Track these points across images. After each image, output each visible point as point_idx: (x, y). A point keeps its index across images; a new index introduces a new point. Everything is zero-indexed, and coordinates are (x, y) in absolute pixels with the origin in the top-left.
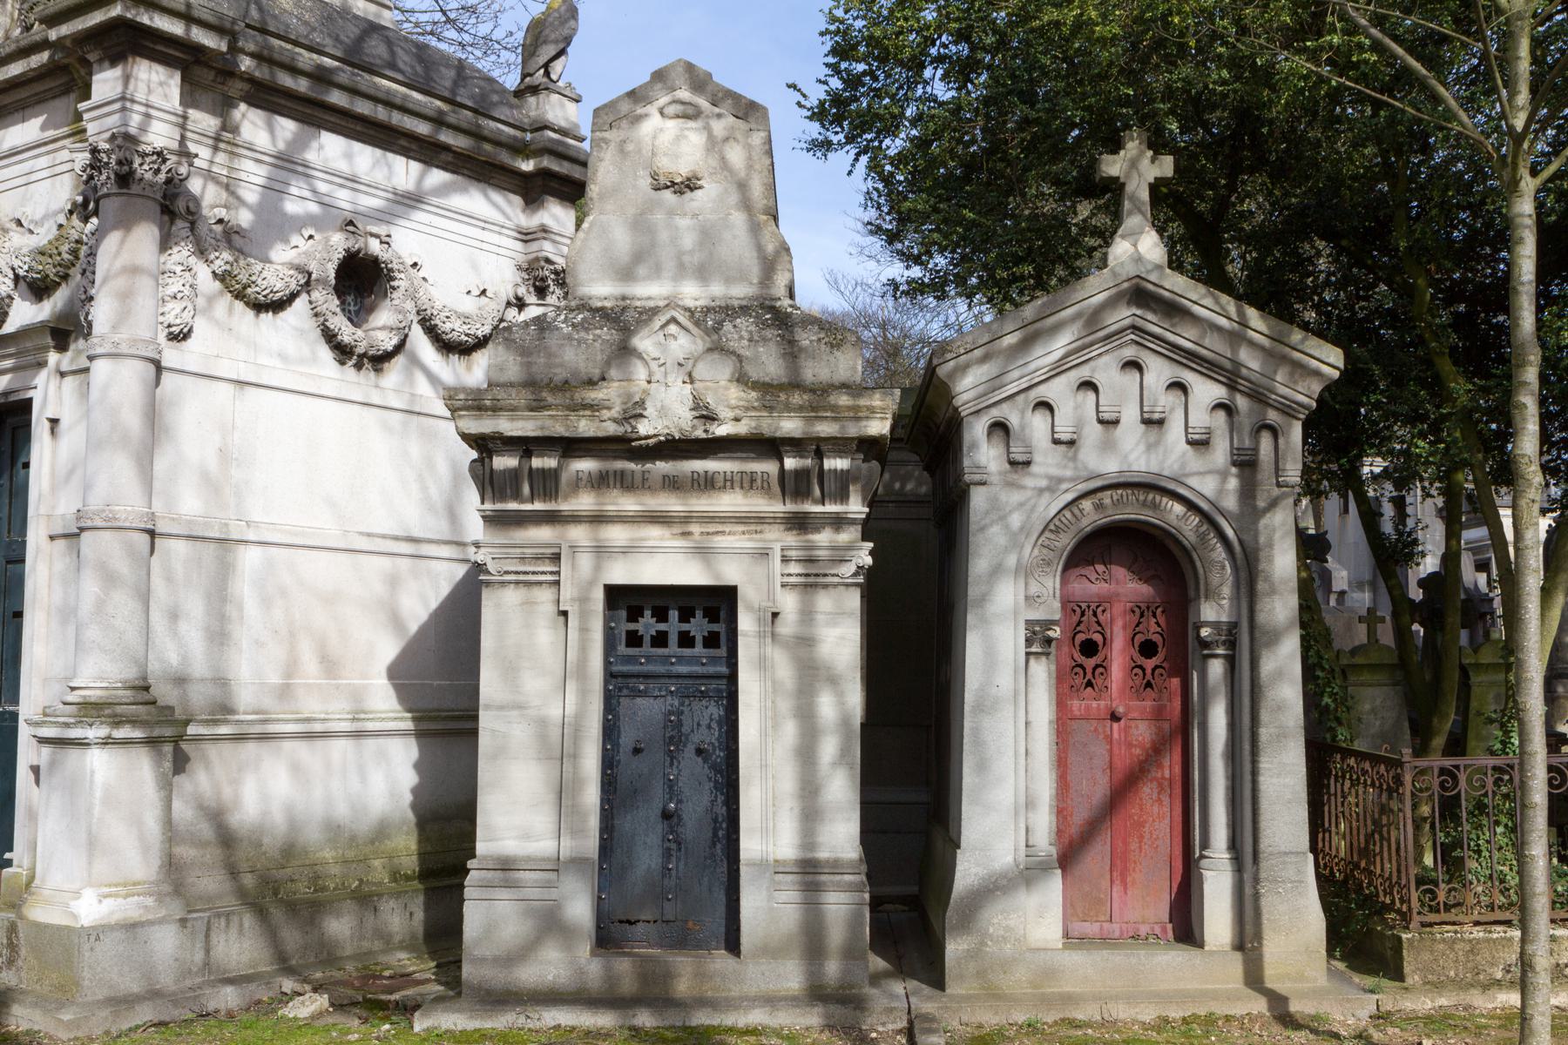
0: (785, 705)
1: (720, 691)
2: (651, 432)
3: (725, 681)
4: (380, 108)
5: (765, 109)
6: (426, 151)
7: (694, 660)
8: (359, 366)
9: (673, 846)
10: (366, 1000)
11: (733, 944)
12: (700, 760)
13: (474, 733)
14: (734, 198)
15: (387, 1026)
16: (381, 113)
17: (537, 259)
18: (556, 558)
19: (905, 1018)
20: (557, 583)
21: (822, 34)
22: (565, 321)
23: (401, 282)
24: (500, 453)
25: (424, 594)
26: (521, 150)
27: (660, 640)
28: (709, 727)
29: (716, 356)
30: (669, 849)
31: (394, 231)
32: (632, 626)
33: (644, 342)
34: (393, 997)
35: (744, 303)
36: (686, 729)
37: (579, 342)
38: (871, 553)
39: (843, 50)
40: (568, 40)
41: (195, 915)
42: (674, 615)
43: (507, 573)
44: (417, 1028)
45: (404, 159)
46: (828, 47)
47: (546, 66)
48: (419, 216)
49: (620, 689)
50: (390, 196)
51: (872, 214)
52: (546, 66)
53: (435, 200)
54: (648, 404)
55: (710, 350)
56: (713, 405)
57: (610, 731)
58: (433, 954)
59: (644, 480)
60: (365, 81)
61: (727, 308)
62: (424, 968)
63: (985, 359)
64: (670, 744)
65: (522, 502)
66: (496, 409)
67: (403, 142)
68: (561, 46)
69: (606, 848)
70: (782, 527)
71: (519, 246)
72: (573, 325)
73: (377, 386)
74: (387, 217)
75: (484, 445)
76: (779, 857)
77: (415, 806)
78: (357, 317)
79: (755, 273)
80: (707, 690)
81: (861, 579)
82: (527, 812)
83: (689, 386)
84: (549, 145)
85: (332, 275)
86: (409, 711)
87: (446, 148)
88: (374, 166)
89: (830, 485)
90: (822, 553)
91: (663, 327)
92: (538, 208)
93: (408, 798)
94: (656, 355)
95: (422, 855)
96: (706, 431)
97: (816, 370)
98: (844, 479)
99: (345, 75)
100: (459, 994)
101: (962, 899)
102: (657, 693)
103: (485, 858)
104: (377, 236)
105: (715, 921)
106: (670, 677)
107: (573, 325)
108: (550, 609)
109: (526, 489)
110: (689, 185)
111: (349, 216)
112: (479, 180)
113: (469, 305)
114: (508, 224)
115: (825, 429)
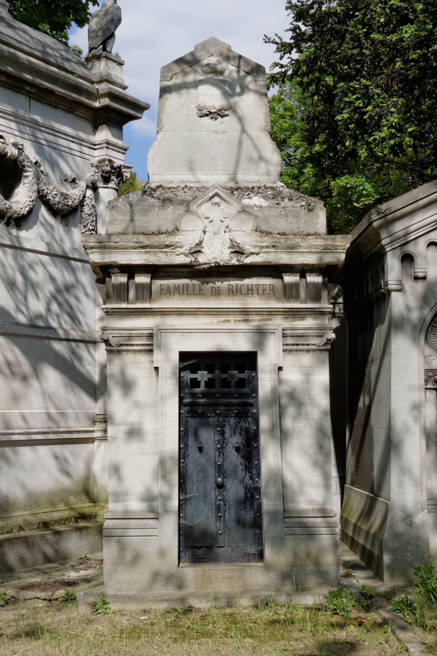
9: (222, 503)
29: (243, 216)
30: (219, 505)
41: (30, 594)
64: (218, 444)
70: (282, 317)
81: (329, 347)
96: (238, 260)
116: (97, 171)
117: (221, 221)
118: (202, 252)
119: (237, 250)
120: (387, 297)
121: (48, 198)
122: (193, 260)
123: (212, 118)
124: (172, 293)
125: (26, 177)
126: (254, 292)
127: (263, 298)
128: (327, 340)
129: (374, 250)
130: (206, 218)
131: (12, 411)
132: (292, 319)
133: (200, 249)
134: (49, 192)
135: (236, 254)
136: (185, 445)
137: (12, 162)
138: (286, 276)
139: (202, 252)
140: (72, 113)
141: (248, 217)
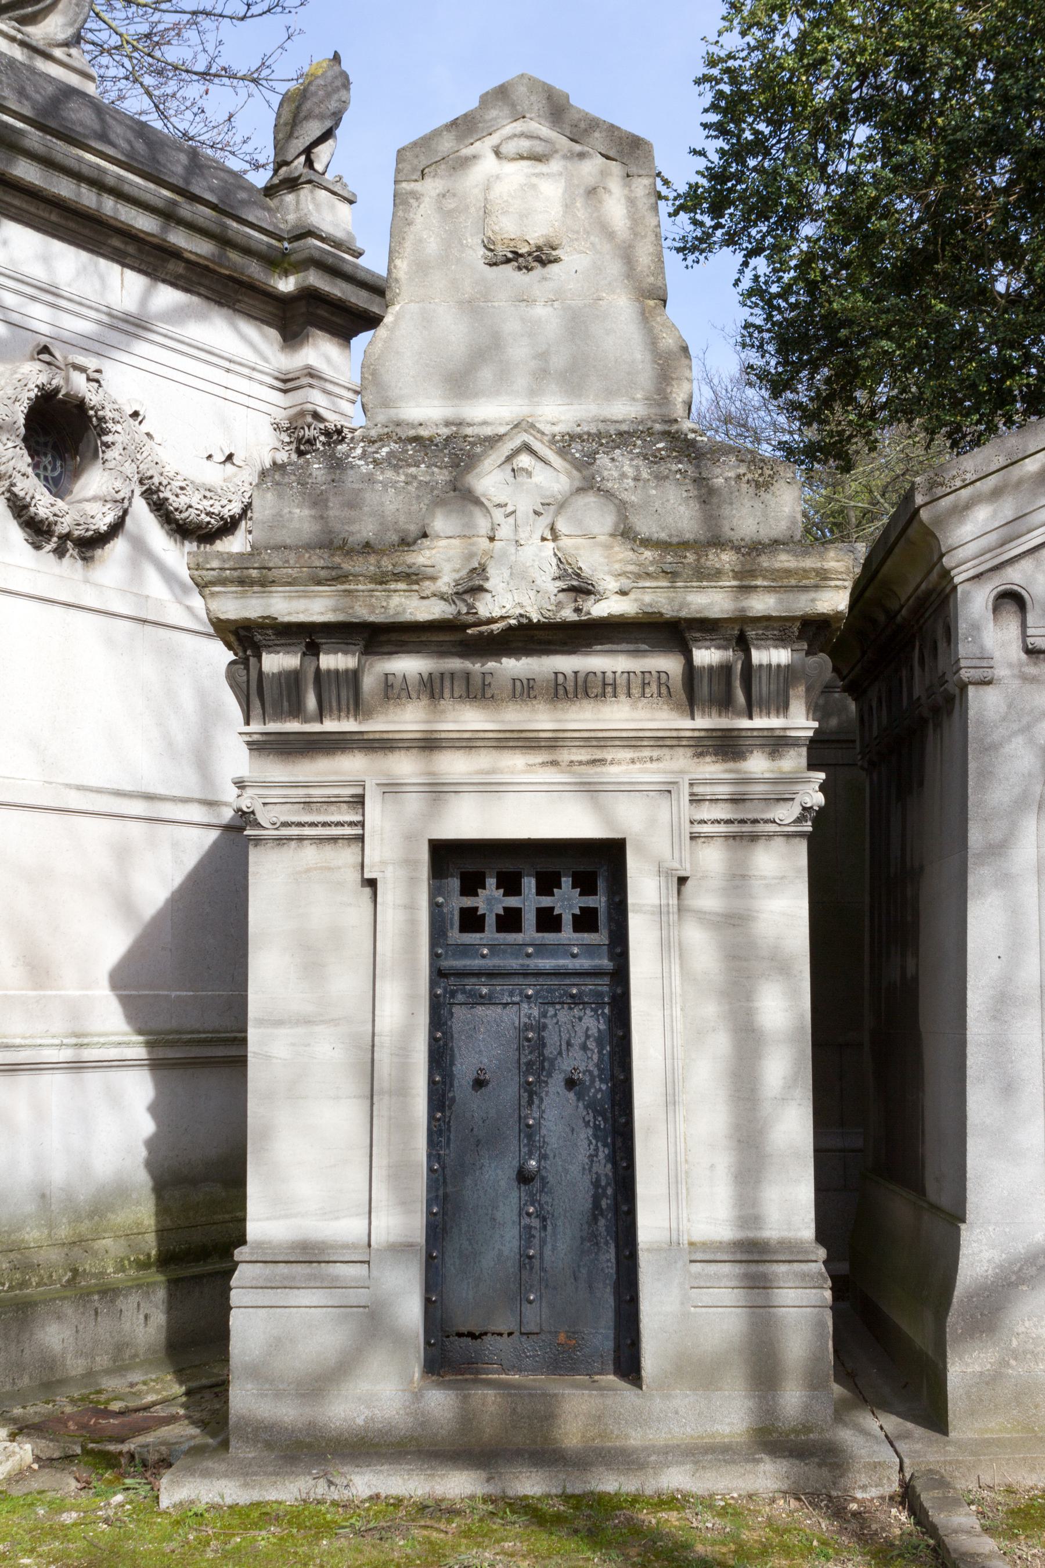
0: (711, 1009)
1: (600, 994)
2: (497, 613)
3: (606, 980)
4: (84, 189)
5: (647, 143)
6: (151, 258)
7: (561, 950)
8: (60, 552)
9: (535, 1223)
10: (87, 1452)
11: (628, 1365)
12: (571, 1095)
13: (241, 1062)
14: (614, 268)
15: (119, 1498)
16: (88, 198)
17: (302, 414)
18: (359, 801)
19: (896, 1477)
20: (361, 838)
21: (698, 82)
22: (364, 456)
23: (119, 435)
24: (272, 648)
25: (162, 868)
26: (279, 262)
27: (510, 921)
28: (584, 1047)
30: (529, 1228)
31: (107, 366)
32: (468, 902)
33: (489, 480)
34: (125, 1448)
35: (624, 427)
36: (550, 1051)
37: (385, 486)
38: (823, 788)
39: (730, 109)
40: (337, 117)
42: (529, 884)
43: (286, 824)
44: (165, 1502)
45: (116, 268)
46: (708, 99)
47: (308, 151)
48: (142, 348)
49: (453, 993)
50: (105, 319)
51: (753, 357)
52: (308, 151)
53: (163, 327)
54: (491, 571)
55: (580, 490)
56: (587, 572)
57: (440, 1056)
58: (181, 1374)
59: (485, 686)
60: (61, 150)
61: (599, 435)
62: (162, 1388)
63: (996, 494)
64: (528, 1072)
65: (306, 721)
66: (264, 583)
67: (116, 242)
68: (328, 124)
69: (438, 1230)
70: (689, 752)
71: (277, 397)
72: (375, 462)
73: (86, 581)
74: (97, 347)
75: (244, 638)
76: (696, 1237)
77: (149, 1165)
78: (58, 487)
79: (645, 376)
80: (581, 994)
82: (331, 1171)
83: (550, 545)
84: (317, 255)
85: (22, 421)
86: (140, 1032)
87: (175, 254)
88: (78, 274)
89: (761, 686)
90: (758, 789)
91: (509, 459)
92: (301, 344)
93: (143, 1153)
94: (502, 499)
95: (161, 1232)
96: (578, 610)
97: (746, 519)
98: (786, 675)
99: (34, 139)
100: (225, 1445)
101: (970, 1297)
102: (506, 999)
103: (259, 1245)
104: (82, 369)
105: (602, 1337)
106: (525, 975)
107: (375, 462)
108: (353, 877)
109: (311, 702)
110: (542, 257)
111: (44, 341)
112: (220, 304)
113: (214, 475)
114: (262, 365)
115: (762, 604)
116: (287, 439)
117: (536, 513)
118: (487, 591)
119: (575, 583)
120: (957, 702)
121: (161, 495)
122: (464, 610)
123: (519, 268)
124: (414, 695)
125: (107, 445)
126: (619, 690)
127: (640, 705)
128: (804, 809)
129: (923, 586)
130: (499, 506)
131: (152, 993)
132: (714, 759)
133: (481, 582)
134: (165, 482)
135: (572, 595)
136: (443, 1077)
137: (75, 411)
138: (699, 648)
139: (487, 591)
140: (229, 307)
141: (603, 500)
